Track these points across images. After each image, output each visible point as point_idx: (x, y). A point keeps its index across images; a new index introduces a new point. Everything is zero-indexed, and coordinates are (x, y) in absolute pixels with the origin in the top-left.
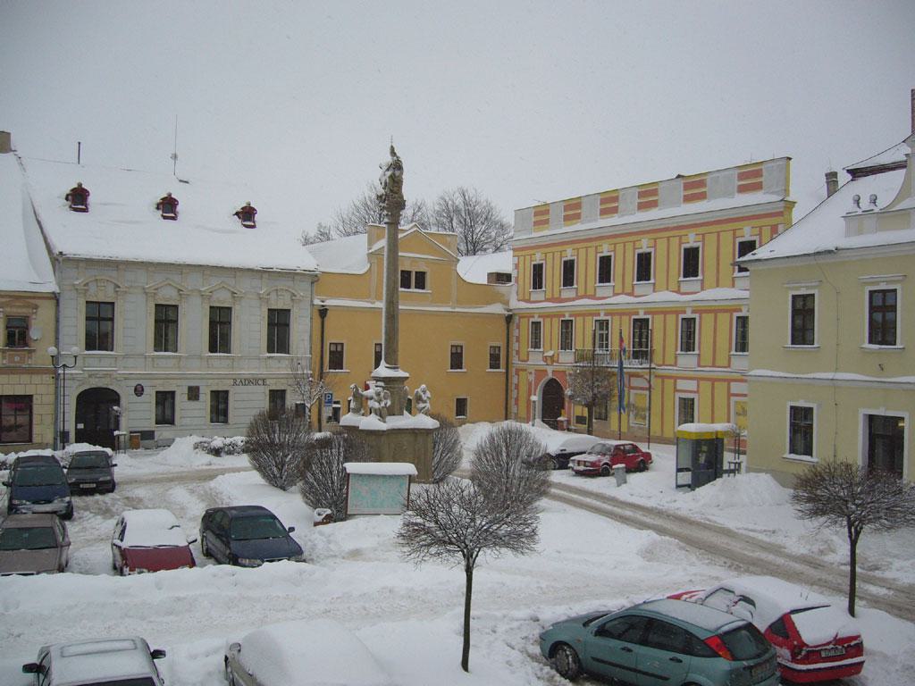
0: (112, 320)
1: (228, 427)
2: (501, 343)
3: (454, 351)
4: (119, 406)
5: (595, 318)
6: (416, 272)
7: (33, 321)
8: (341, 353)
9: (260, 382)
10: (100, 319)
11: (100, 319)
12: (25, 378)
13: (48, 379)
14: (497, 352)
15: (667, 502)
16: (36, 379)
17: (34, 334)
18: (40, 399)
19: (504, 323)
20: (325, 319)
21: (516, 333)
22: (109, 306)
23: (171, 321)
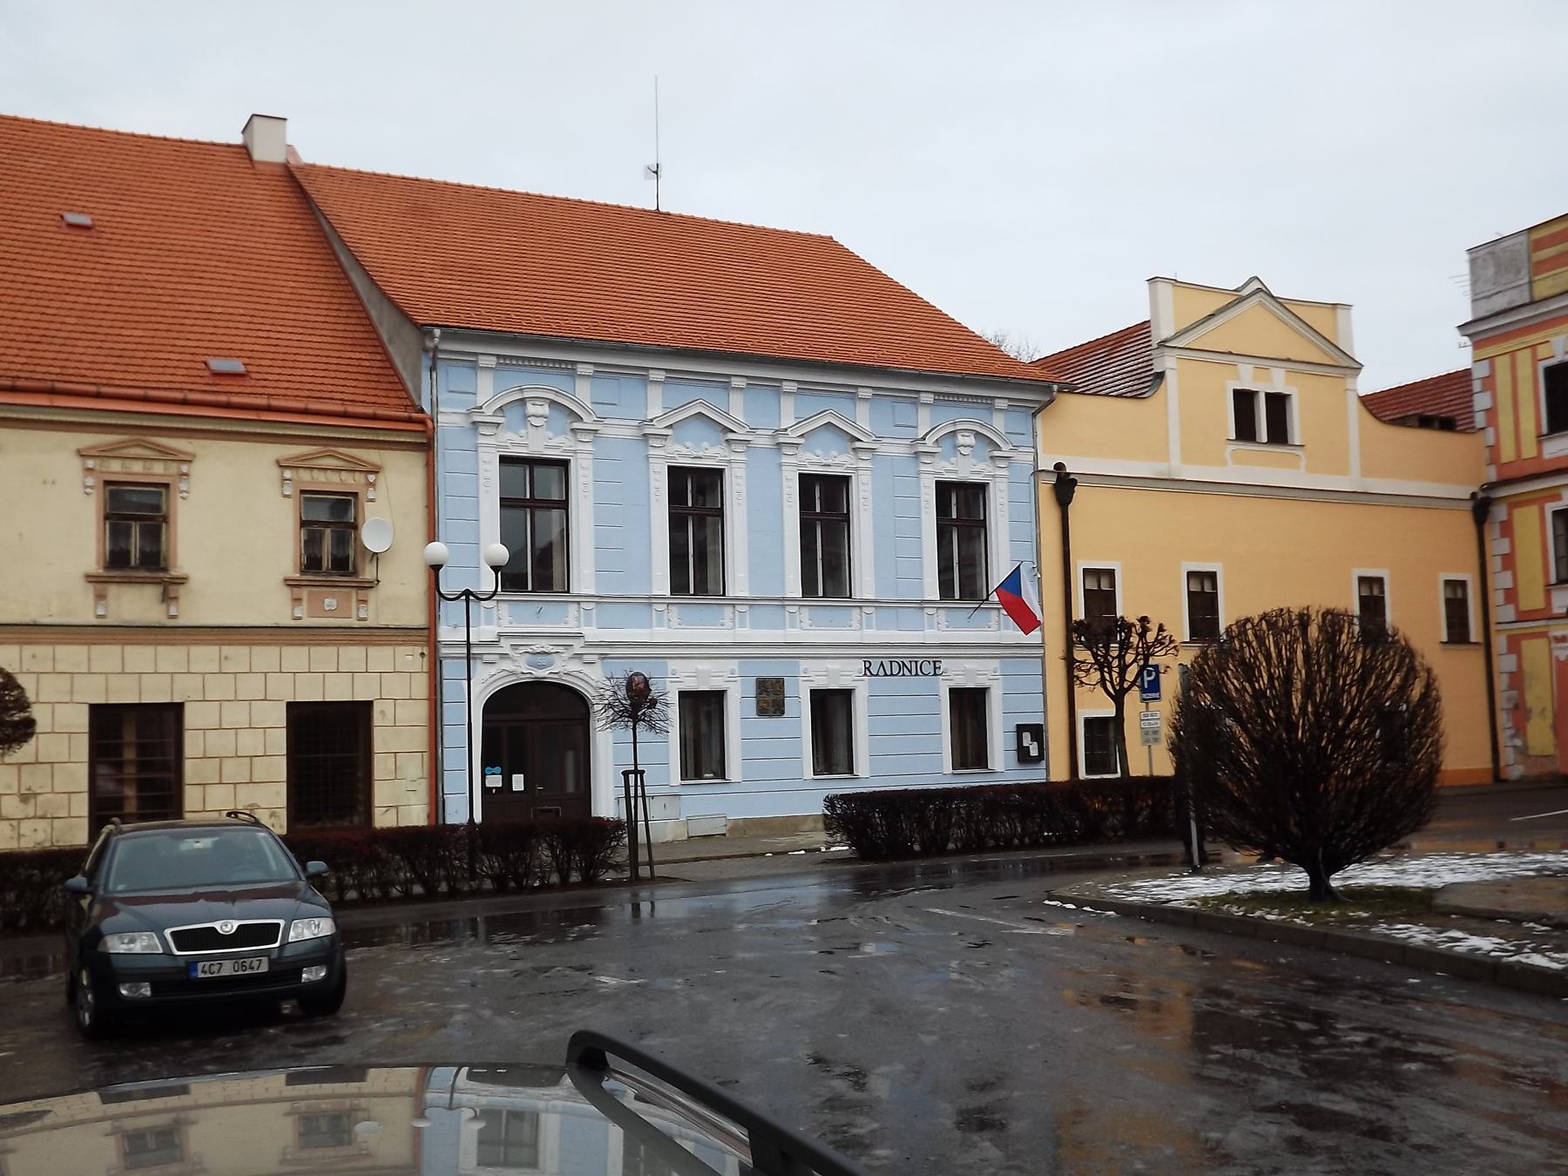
0: (564, 505)
1: (725, 789)
2: (1471, 578)
3: (1195, 588)
4: (1515, 747)
5: (1550, 507)
6: (1267, 395)
7: (368, 506)
8: (1213, 597)
9: (928, 668)
10: (537, 504)
11: (537, 504)
12: (352, 655)
13: (411, 658)
14: (1459, 594)
15: (1206, 1004)
16: (381, 656)
17: (372, 538)
18: (390, 714)
19: (1464, 523)
20: (1486, 527)
21: (1503, 546)
22: (554, 472)
23: (550, 505)
